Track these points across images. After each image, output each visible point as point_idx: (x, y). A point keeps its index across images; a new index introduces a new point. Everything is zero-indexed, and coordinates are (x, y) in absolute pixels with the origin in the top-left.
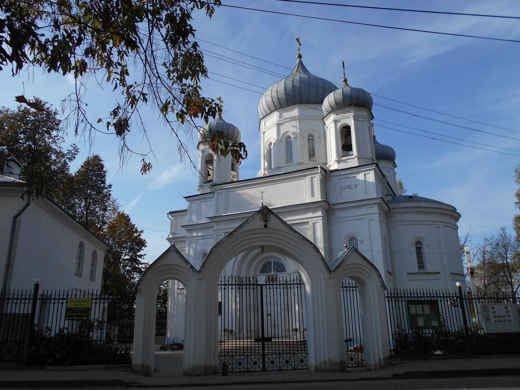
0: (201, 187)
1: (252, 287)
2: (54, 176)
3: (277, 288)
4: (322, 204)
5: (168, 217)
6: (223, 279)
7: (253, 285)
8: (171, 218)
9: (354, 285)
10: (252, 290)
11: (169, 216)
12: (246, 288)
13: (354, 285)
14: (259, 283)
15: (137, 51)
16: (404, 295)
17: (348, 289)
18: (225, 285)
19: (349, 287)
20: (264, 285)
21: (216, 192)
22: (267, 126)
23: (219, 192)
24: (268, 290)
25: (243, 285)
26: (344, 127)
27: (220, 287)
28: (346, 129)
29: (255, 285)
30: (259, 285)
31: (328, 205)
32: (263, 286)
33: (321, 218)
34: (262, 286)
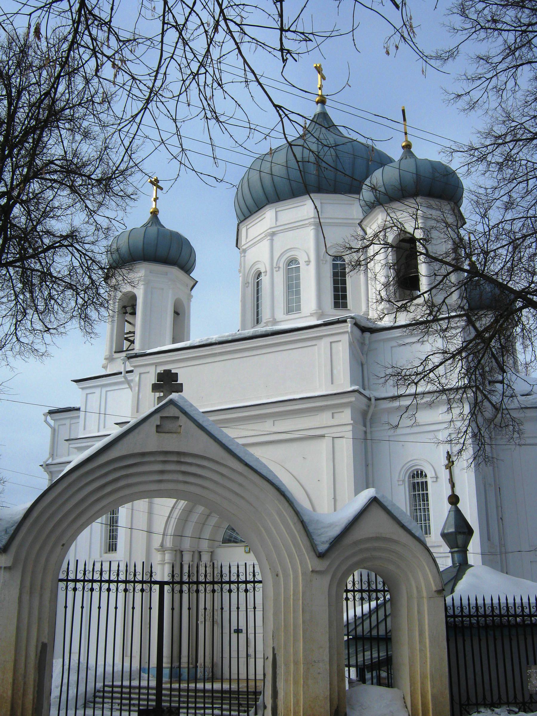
0: (110, 359)
1: (122, 586)
2: (24, 240)
3: (246, 591)
4: (353, 399)
5: (46, 421)
6: (209, 570)
7: (142, 582)
8: (52, 423)
9: (380, 587)
10: (138, 595)
11: (49, 418)
12: (109, 590)
13: (380, 587)
14: (157, 577)
15: (30, 102)
16: (523, 610)
17: (350, 595)
18: (126, 582)
19: (354, 591)
20: (167, 583)
21: (137, 371)
22: (250, 237)
23: (142, 370)
24: (70, 593)
25: (189, 583)
26: (403, 241)
27: (62, 585)
28: (407, 245)
29: (146, 582)
30: (156, 583)
31: (365, 400)
32: (166, 587)
33: (350, 428)
34: (162, 584)
